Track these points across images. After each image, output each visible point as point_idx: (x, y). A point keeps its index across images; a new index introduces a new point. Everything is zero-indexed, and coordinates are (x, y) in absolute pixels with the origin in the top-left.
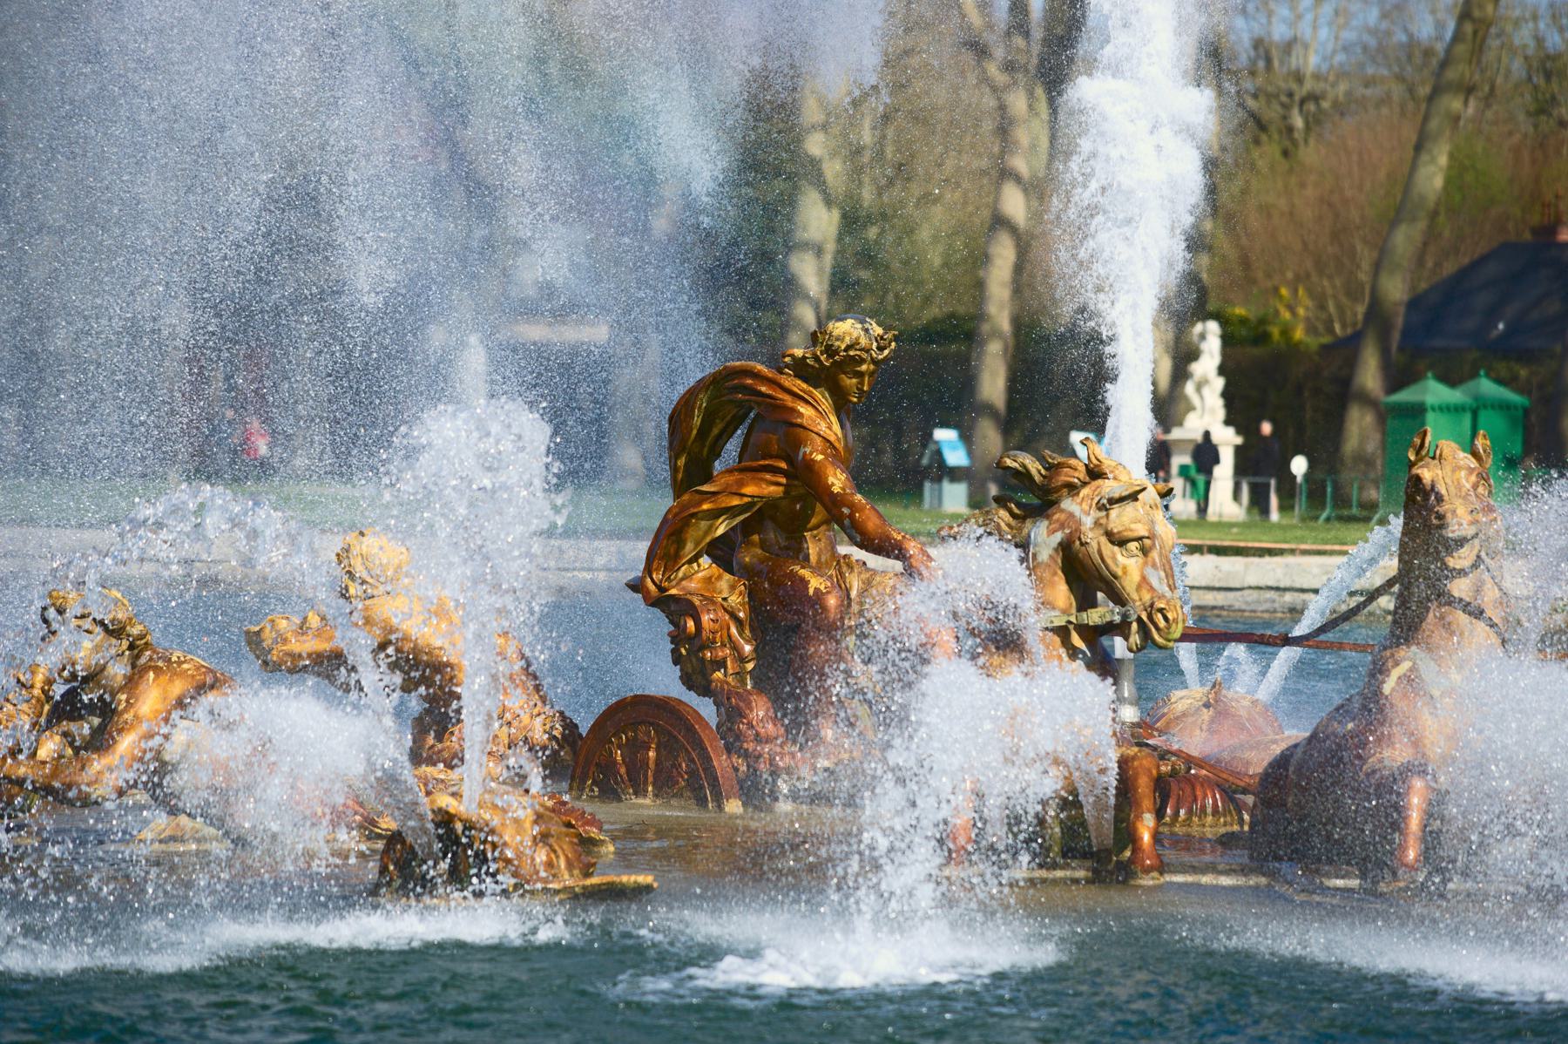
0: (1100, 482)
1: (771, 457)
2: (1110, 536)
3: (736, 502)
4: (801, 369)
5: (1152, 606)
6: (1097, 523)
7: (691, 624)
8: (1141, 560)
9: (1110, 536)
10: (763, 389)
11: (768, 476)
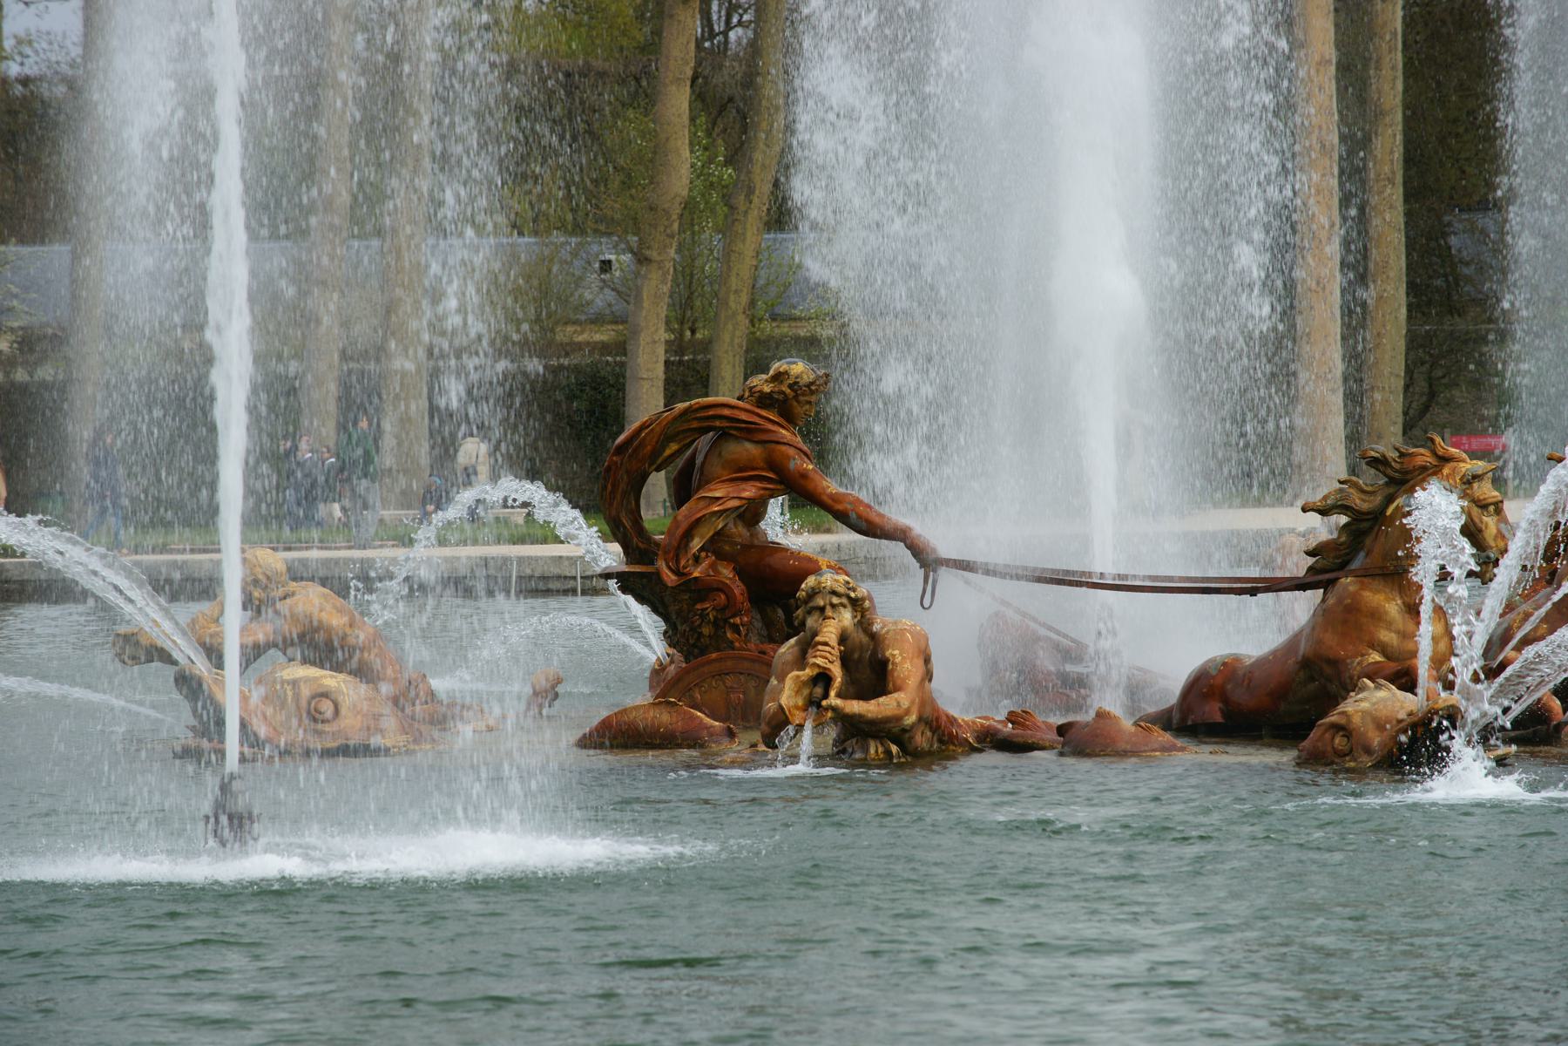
3: (735, 503)
10: (744, 416)
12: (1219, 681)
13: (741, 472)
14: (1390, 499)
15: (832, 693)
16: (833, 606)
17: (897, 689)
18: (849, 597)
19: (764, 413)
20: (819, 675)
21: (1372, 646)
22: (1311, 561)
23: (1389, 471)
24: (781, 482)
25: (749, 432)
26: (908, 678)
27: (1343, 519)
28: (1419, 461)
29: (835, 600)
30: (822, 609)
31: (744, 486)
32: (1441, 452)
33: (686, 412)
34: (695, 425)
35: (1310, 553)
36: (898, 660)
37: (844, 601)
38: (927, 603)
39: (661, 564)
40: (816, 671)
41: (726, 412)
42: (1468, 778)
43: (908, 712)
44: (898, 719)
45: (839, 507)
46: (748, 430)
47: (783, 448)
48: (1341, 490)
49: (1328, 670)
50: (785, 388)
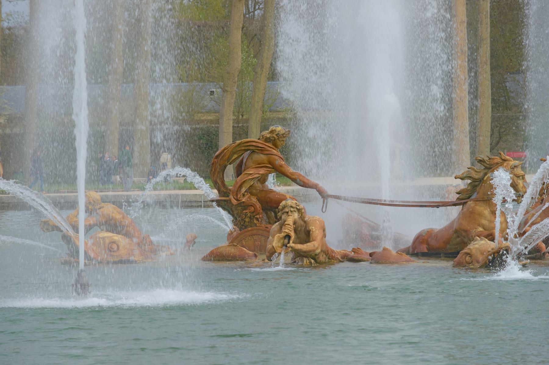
1: (264, 164)
3: (257, 176)
10: (260, 145)
11: (265, 169)
12: (426, 238)
13: (260, 165)
14: (486, 174)
15: (291, 242)
16: (291, 211)
17: (313, 240)
18: (297, 208)
19: (267, 144)
20: (286, 235)
21: (479, 225)
22: (458, 196)
23: (485, 165)
24: (273, 168)
25: (262, 150)
27: (469, 181)
28: (496, 161)
29: (292, 209)
31: (260, 169)
32: (503, 158)
33: (239, 144)
34: (243, 148)
35: (458, 193)
36: (314, 230)
37: (295, 209)
38: (324, 210)
39: (231, 197)
40: (285, 234)
41: (254, 144)
42: (513, 271)
44: (314, 251)
46: (262, 150)
47: (274, 156)
48: (468, 171)
49: (464, 234)
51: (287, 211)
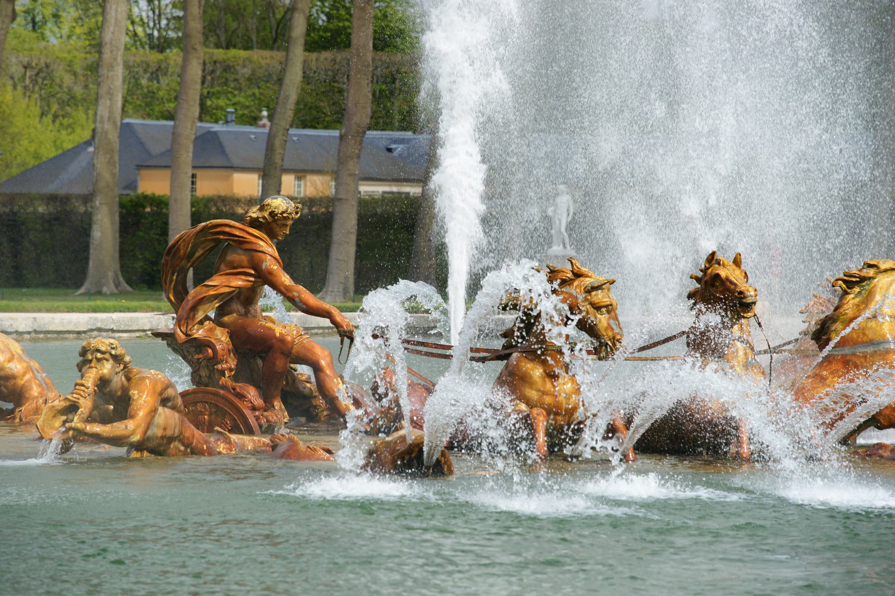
0: (582, 279)
1: (243, 267)
2: (592, 304)
3: (227, 290)
4: (255, 223)
5: (614, 338)
6: (586, 299)
7: (210, 351)
8: (607, 316)
9: (592, 304)
10: (237, 233)
11: (243, 277)
18: (111, 354)
20: (71, 406)
24: (260, 277)
26: (139, 409)
29: (99, 355)
30: (91, 361)
37: (107, 356)
40: (68, 404)
41: (227, 229)
43: (133, 433)
45: (289, 294)
47: (260, 254)
50: (266, 214)
51: (90, 357)
